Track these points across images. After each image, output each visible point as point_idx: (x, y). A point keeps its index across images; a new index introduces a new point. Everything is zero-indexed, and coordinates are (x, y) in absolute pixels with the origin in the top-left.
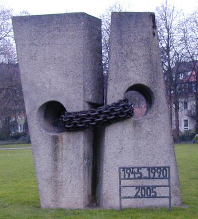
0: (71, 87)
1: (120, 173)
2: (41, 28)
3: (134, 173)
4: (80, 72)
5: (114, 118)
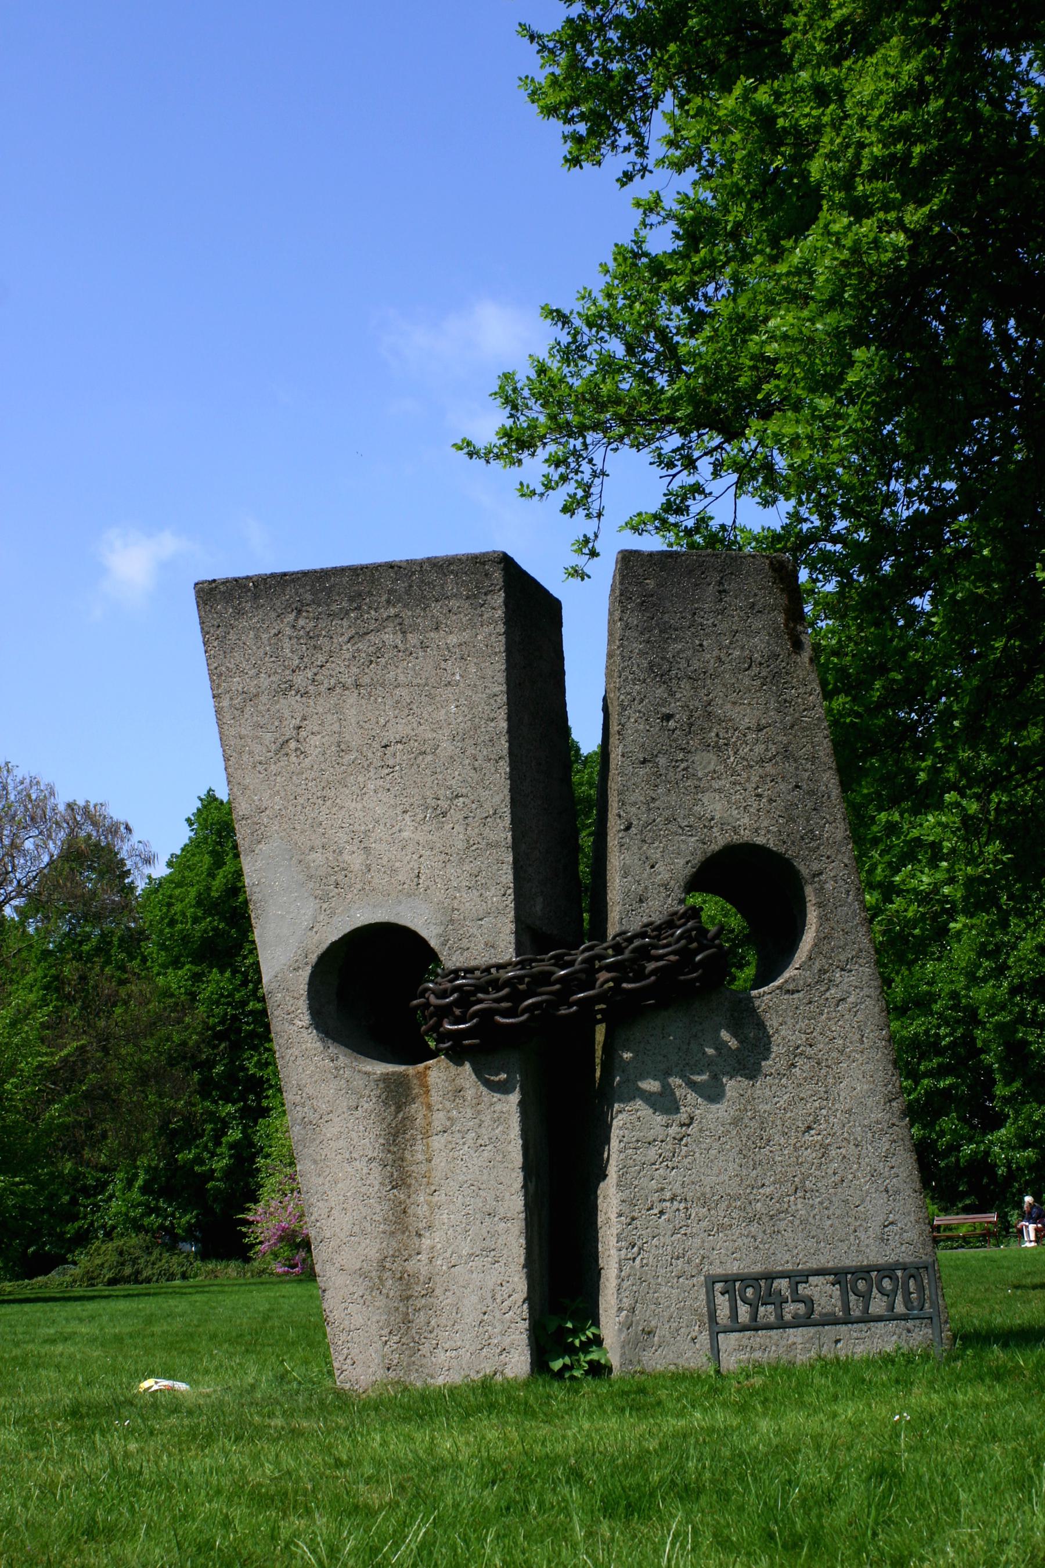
0: (461, 861)
2: (322, 624)
4: (497, 799)
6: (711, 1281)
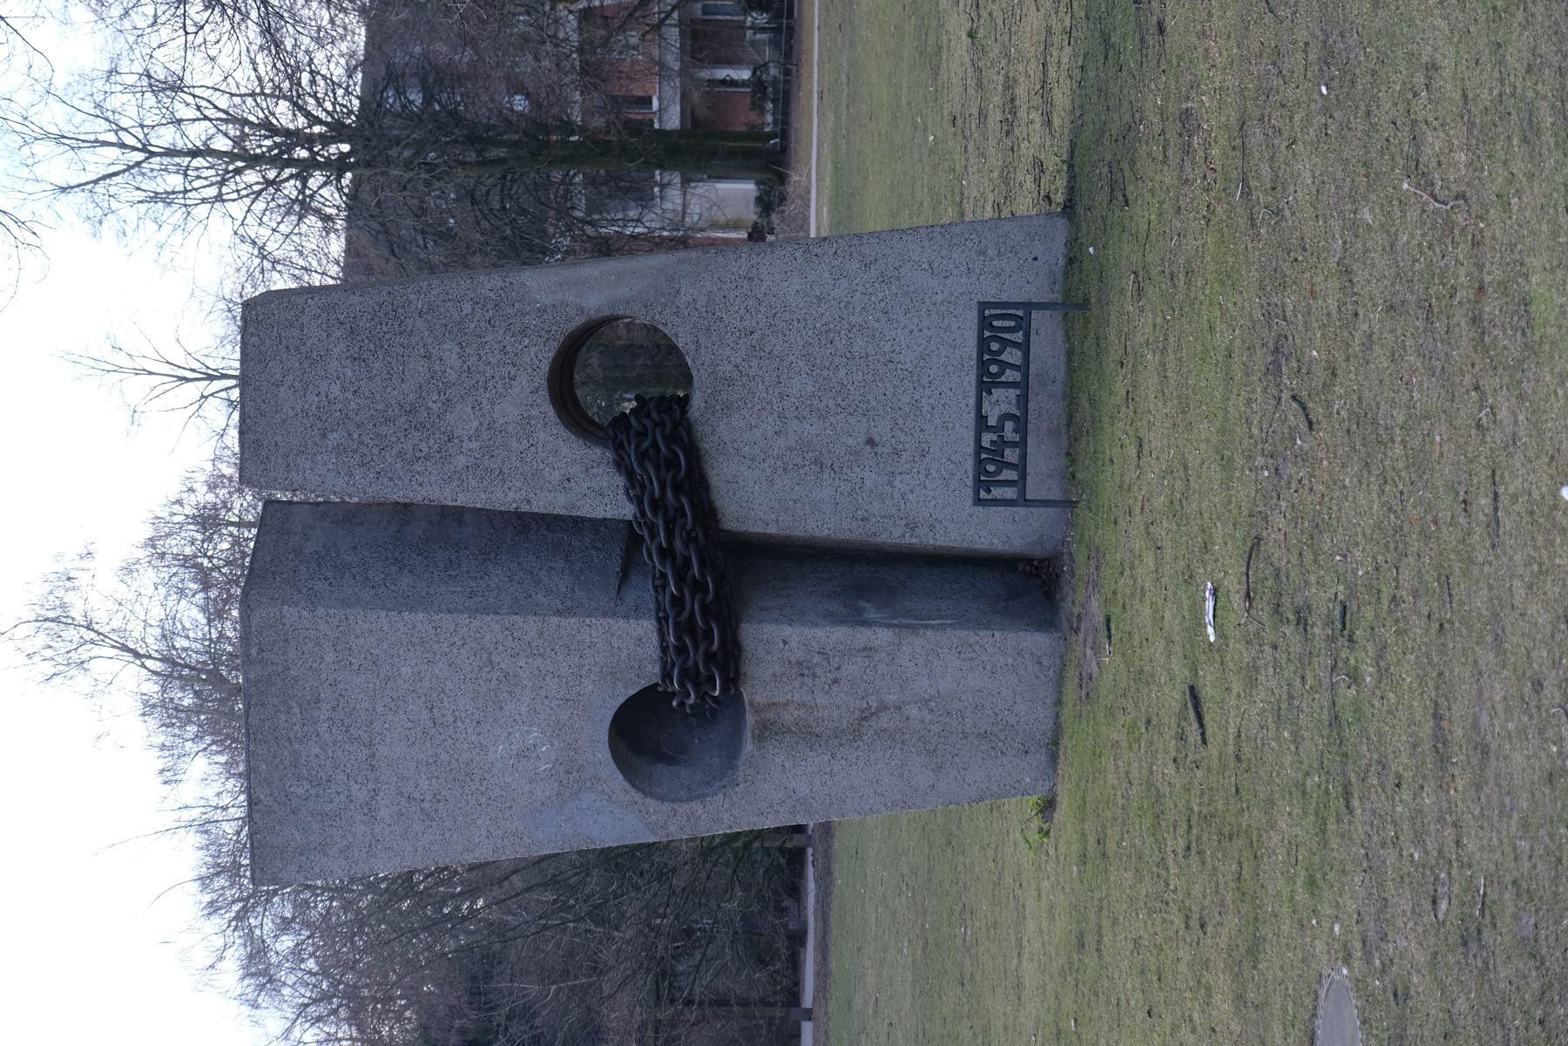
3: (1002, 443)
4: (496, 627)
5: (691, 502)
6: (978, 501)
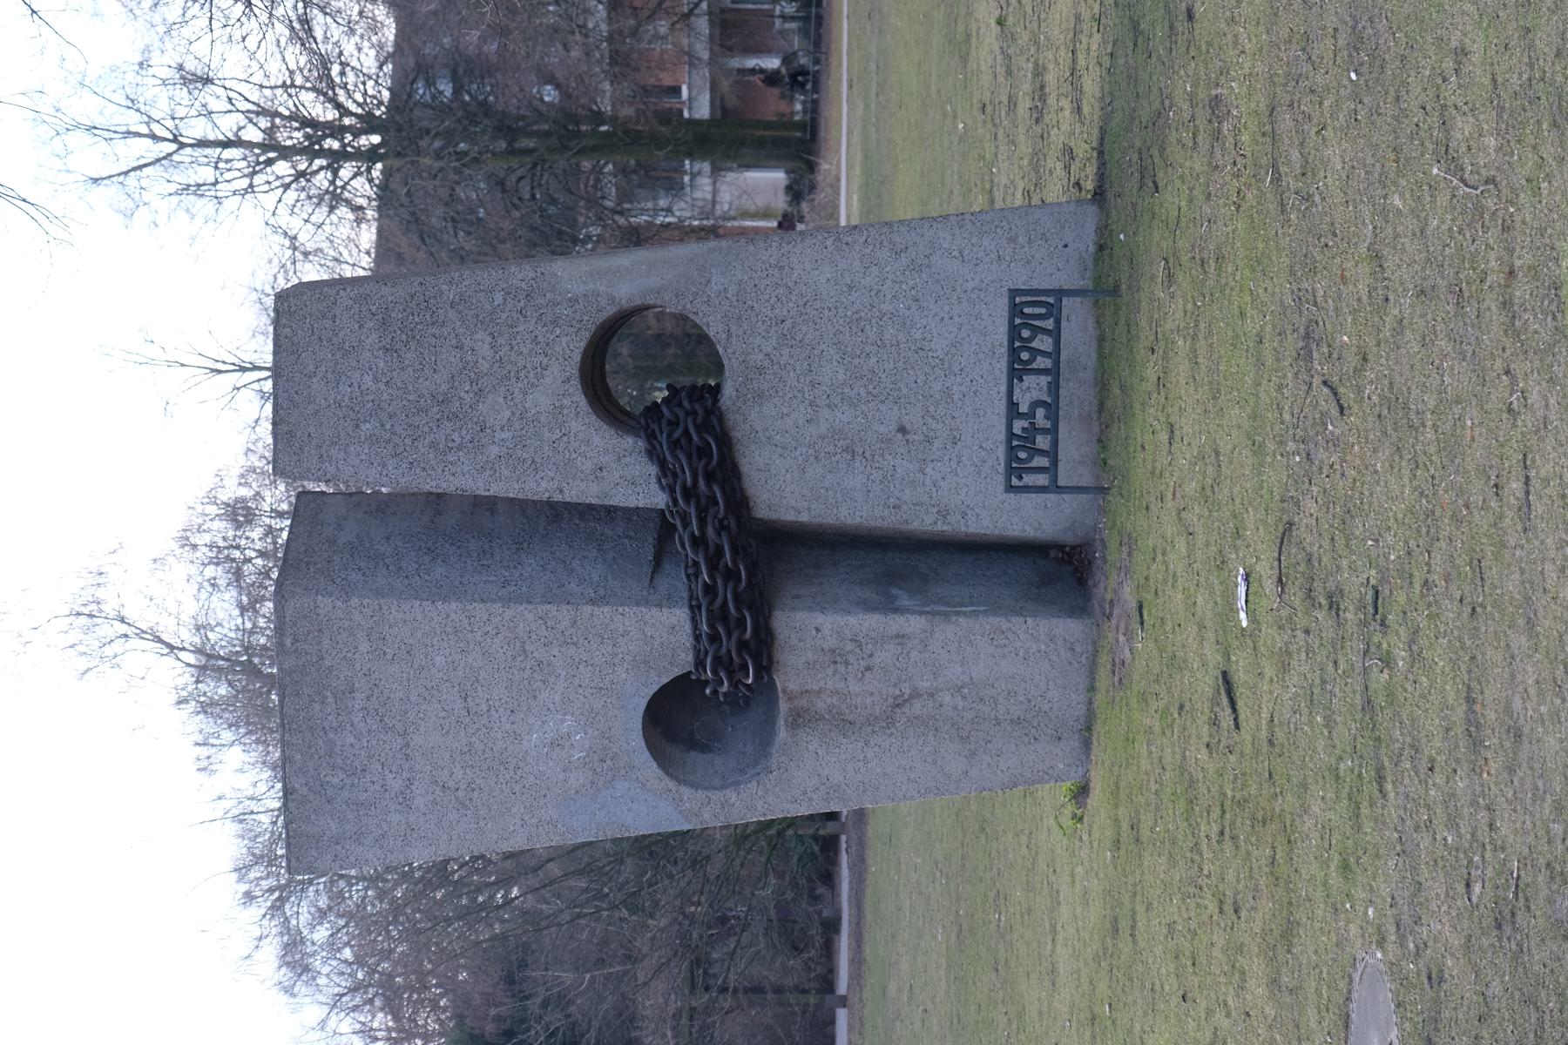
1: (1027, 489)
6: (1010, 488)
